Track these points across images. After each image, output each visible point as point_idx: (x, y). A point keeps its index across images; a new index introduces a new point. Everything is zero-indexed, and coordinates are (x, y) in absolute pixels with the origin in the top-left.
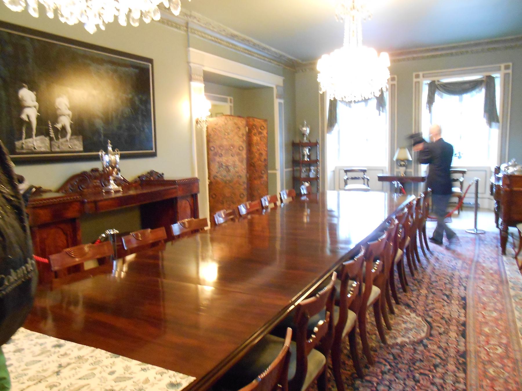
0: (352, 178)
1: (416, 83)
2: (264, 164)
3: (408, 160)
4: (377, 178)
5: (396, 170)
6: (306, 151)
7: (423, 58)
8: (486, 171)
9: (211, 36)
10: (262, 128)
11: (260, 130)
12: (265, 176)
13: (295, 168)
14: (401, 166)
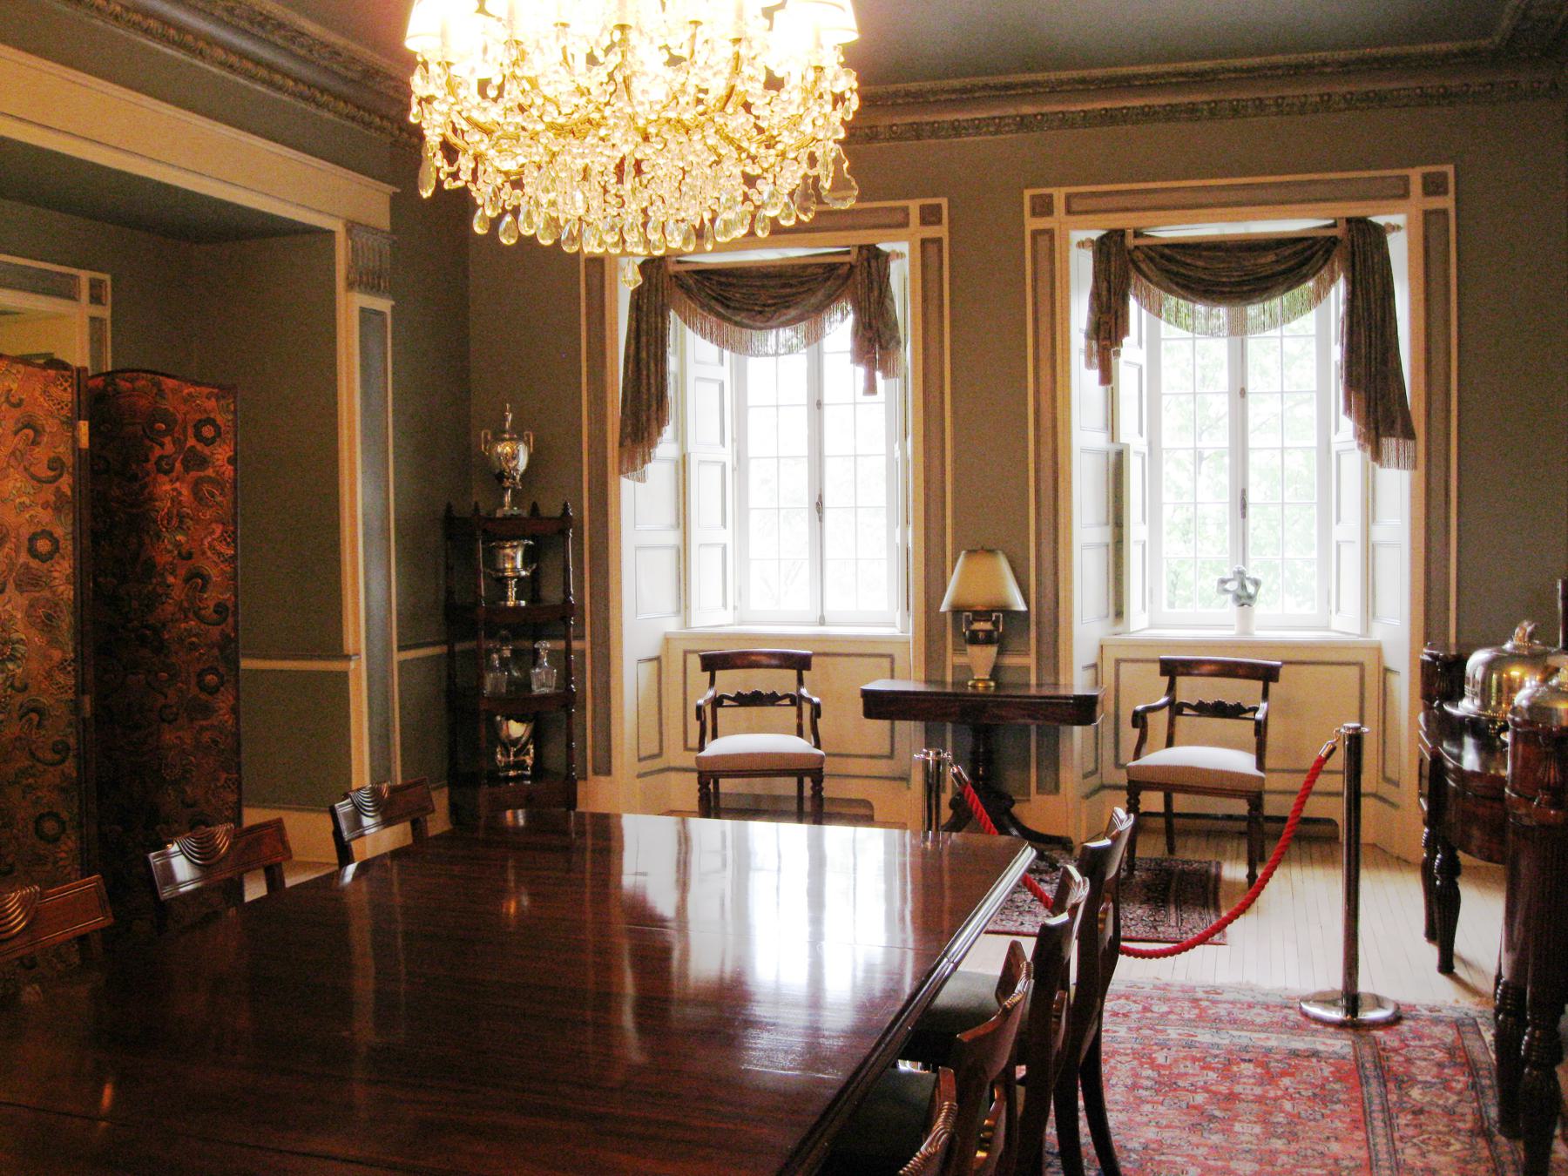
0: (743, 700)
1: (1036, 234)
2: (215, 632)
3: (1008, 613)
5: (952, 659)
6: (513, 559)
7: (1065, 121)
8: (1361, 665)
10: (208, 431)
11: (191, 442)
13: (458, 647)
14: (974, 639)
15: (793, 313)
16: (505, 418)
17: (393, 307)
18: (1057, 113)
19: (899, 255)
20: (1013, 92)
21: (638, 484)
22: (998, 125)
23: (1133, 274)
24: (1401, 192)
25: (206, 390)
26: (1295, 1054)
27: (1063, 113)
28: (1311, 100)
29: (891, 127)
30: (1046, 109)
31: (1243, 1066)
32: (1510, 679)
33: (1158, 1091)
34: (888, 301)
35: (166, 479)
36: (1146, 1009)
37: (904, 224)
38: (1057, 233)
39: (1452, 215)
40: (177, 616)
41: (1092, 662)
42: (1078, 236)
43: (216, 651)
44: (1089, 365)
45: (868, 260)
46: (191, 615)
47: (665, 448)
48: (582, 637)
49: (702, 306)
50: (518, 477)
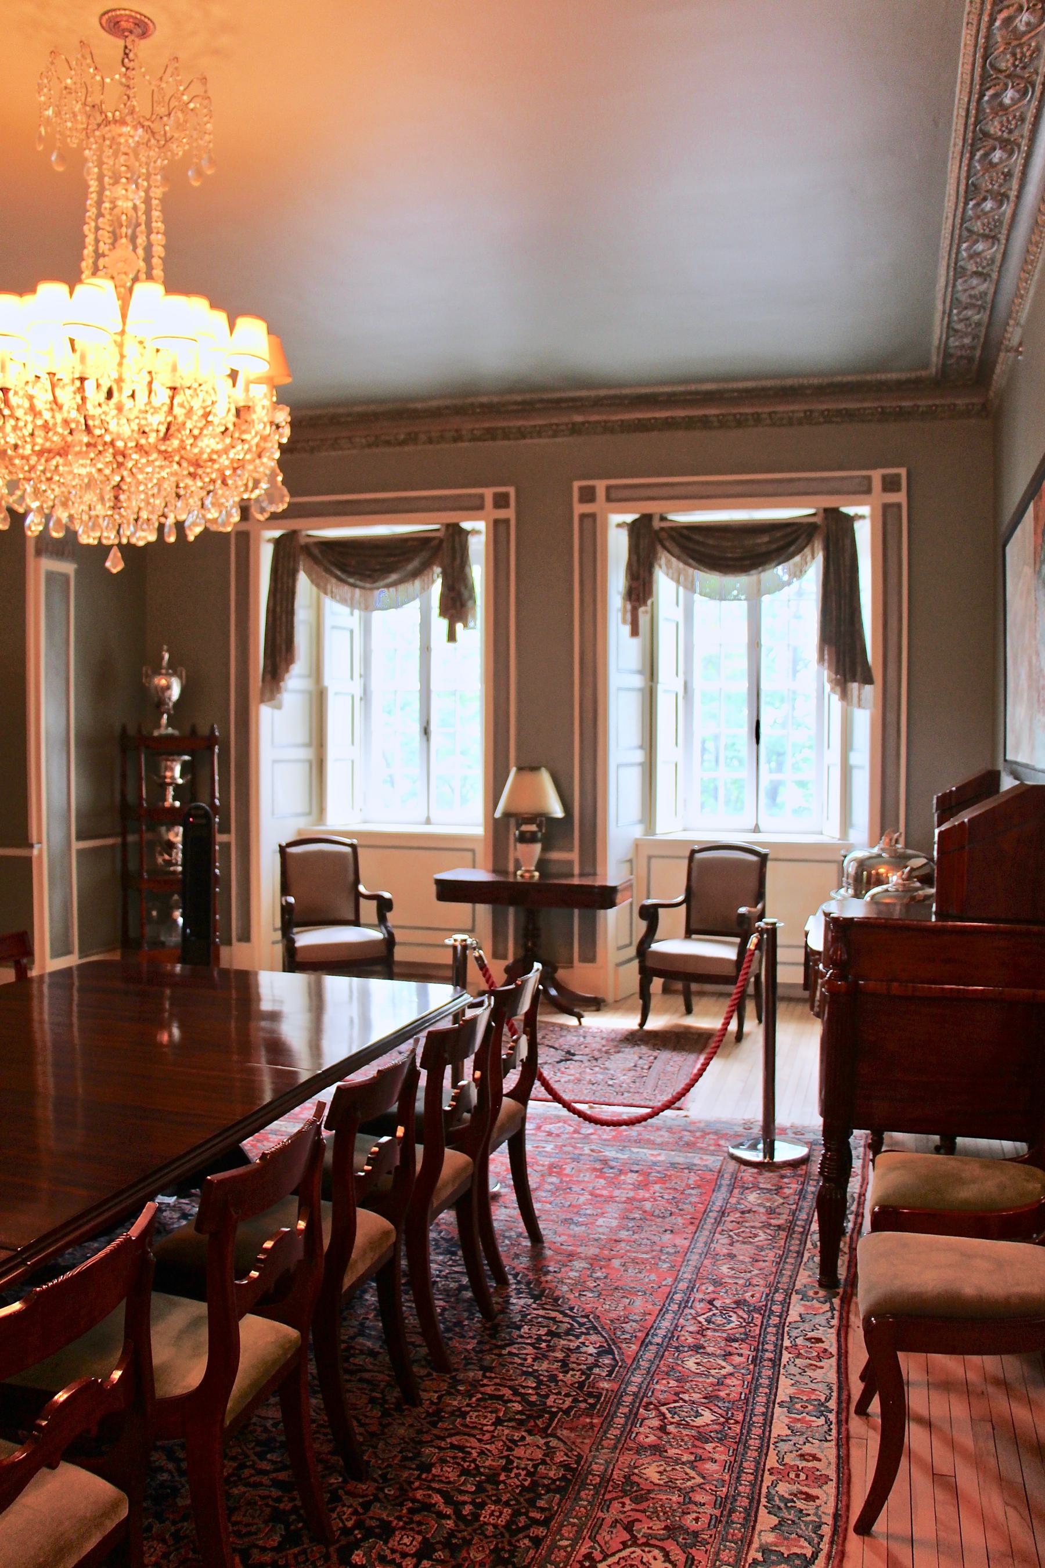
1: (583, 517)
4: (433, 889)
6: (172, 770)
7: (608, 428)
15: (394, 577)
16: (162, 658)
19: (478, 532)
22: (555, 431)
23: (659, 549)
24: (865, 488)
26: (673, 1165)
28: (796, 415)
29: (473, 430)
31: (630, 1175)
32: (878, 874)
33: (553, 1193)
34: (467, 569)
36: (576, 1132)
37: (481, 507)
39: (513, 523)
41: (628, 858)
42: (616, 518)
44: (624, 622)
49: (327, 570)
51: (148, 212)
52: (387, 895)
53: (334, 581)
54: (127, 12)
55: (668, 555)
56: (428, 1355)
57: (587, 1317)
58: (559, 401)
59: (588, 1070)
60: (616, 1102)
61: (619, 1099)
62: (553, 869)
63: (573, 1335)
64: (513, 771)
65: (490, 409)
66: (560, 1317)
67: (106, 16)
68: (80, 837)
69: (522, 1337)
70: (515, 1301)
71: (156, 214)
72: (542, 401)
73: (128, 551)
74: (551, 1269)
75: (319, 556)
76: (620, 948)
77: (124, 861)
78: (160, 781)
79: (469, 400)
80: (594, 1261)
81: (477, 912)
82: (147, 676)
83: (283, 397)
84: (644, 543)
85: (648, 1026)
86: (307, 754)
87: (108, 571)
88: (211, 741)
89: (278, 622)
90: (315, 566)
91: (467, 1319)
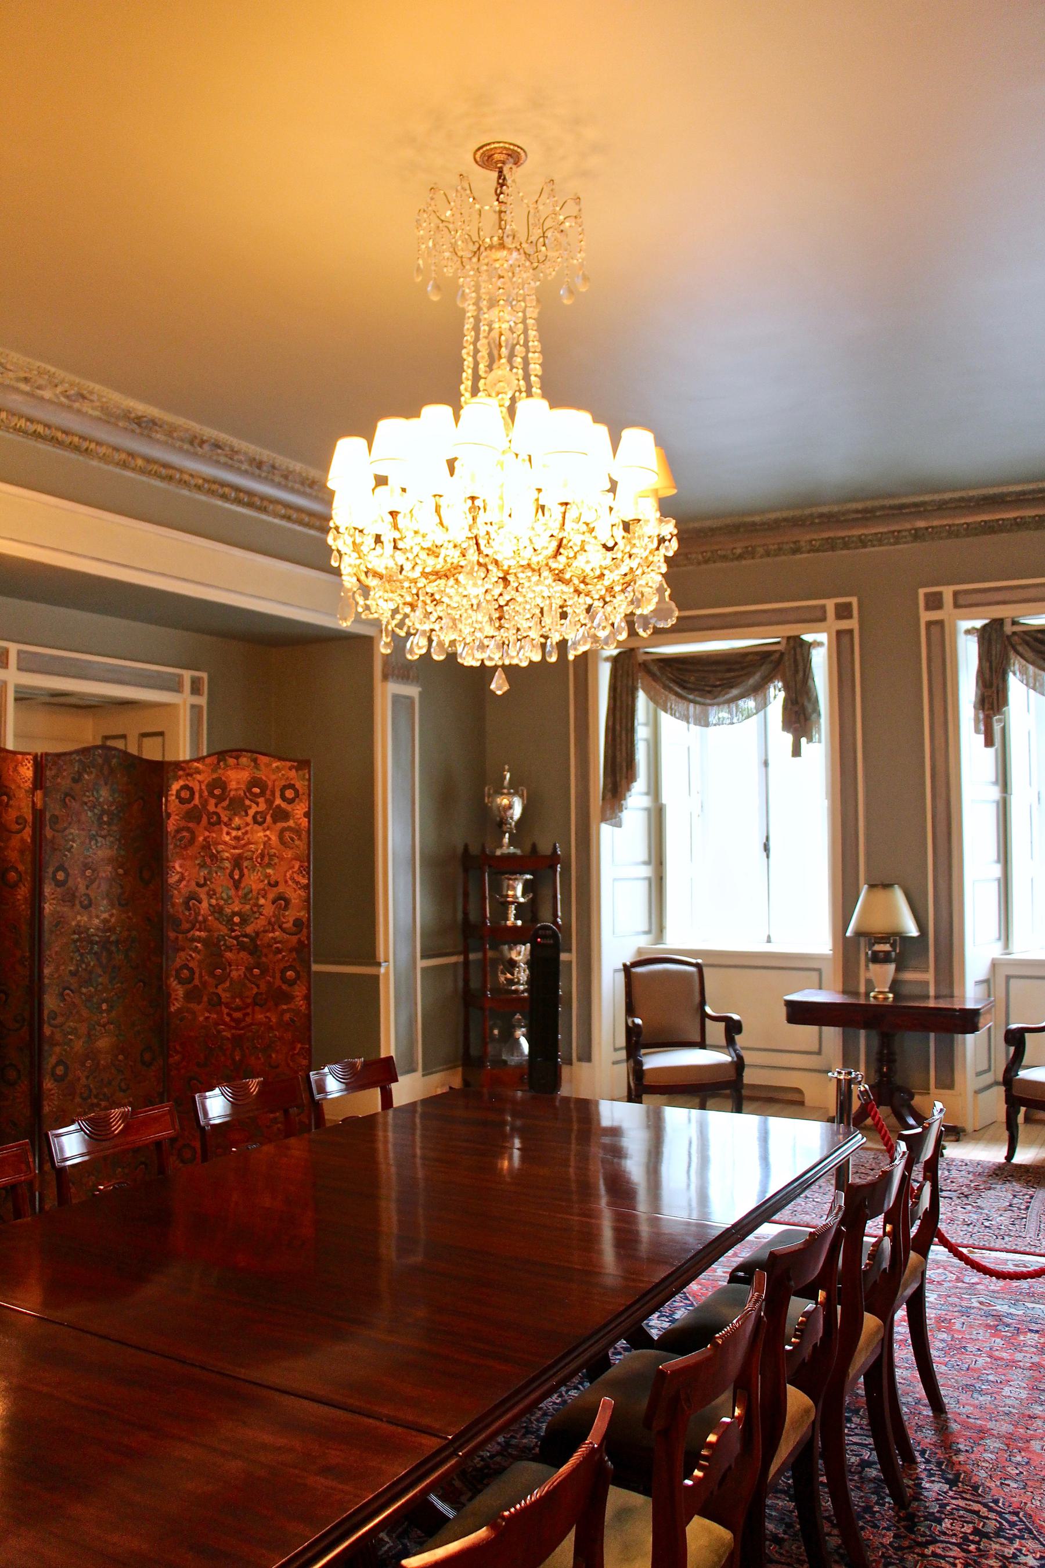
1: (929, 624)
4: (783, 1011)
6: (514, 889)
7: (953, 532)
9: (80, 437)
10: (289, 794)
11: (278, 801)
12: (299, 991)
15: (735, 692)
17: (420, 693)
18: (945, 525)
19: (820, 644)
20: (907, 510)
21: (615, 828)
22: (897, 538)
23: (1012, 654)
25: (289, 764)
27: (950, 526)
29: (811, 541)
30: (936, 523)
31: (1029, 1335)
35: (260, 828)
36: (958, 1280)
37: (823, 619)
38: (947, 624)
40: (267, 928)
42: (965, 625)
43: (294, 955)
44: (977, 731)
45: (794, 649)
46: (276, 927)
47: (637, 798)
48: (569, 950)
49: (666, 687)
50: (513, 824)
51: (525, 332)
52: (736, 1017)
53: (673, 697)
54: (501, 145)
55: (1021, 660)
56: (839, 1547)
57: (1017, 1514)
58: (902, 507)
59: (959, 1208)
60: (997, 1246)
61: (999, 1243)
62: (906, 990)
63: (1005, 1538)
64: (864, 890)
65: (829, 519)
66: (984, 1511)
67: (481, 151)
68: (423, 957)
69: (945, 1534)
70: (927, 1485)
71: (532, 333)
72: (883, 508)
73: (511, 671)
74: (961, 1446)
75: (658, 673)
76: (979, 1074)
77: (466, 981)
78: (502, 900)
79: (807, 512)
80: (1009, 1440)
81: (824, 1036)
82: (489, 796)
83: (666, 508)
84: (996, 649)
85: (1018, 1159)
86: (646, 871)
87: (493, 693)
88: (553, 860)
89: (618, 740)
90: (654, 684)
91: (877, 1503)
